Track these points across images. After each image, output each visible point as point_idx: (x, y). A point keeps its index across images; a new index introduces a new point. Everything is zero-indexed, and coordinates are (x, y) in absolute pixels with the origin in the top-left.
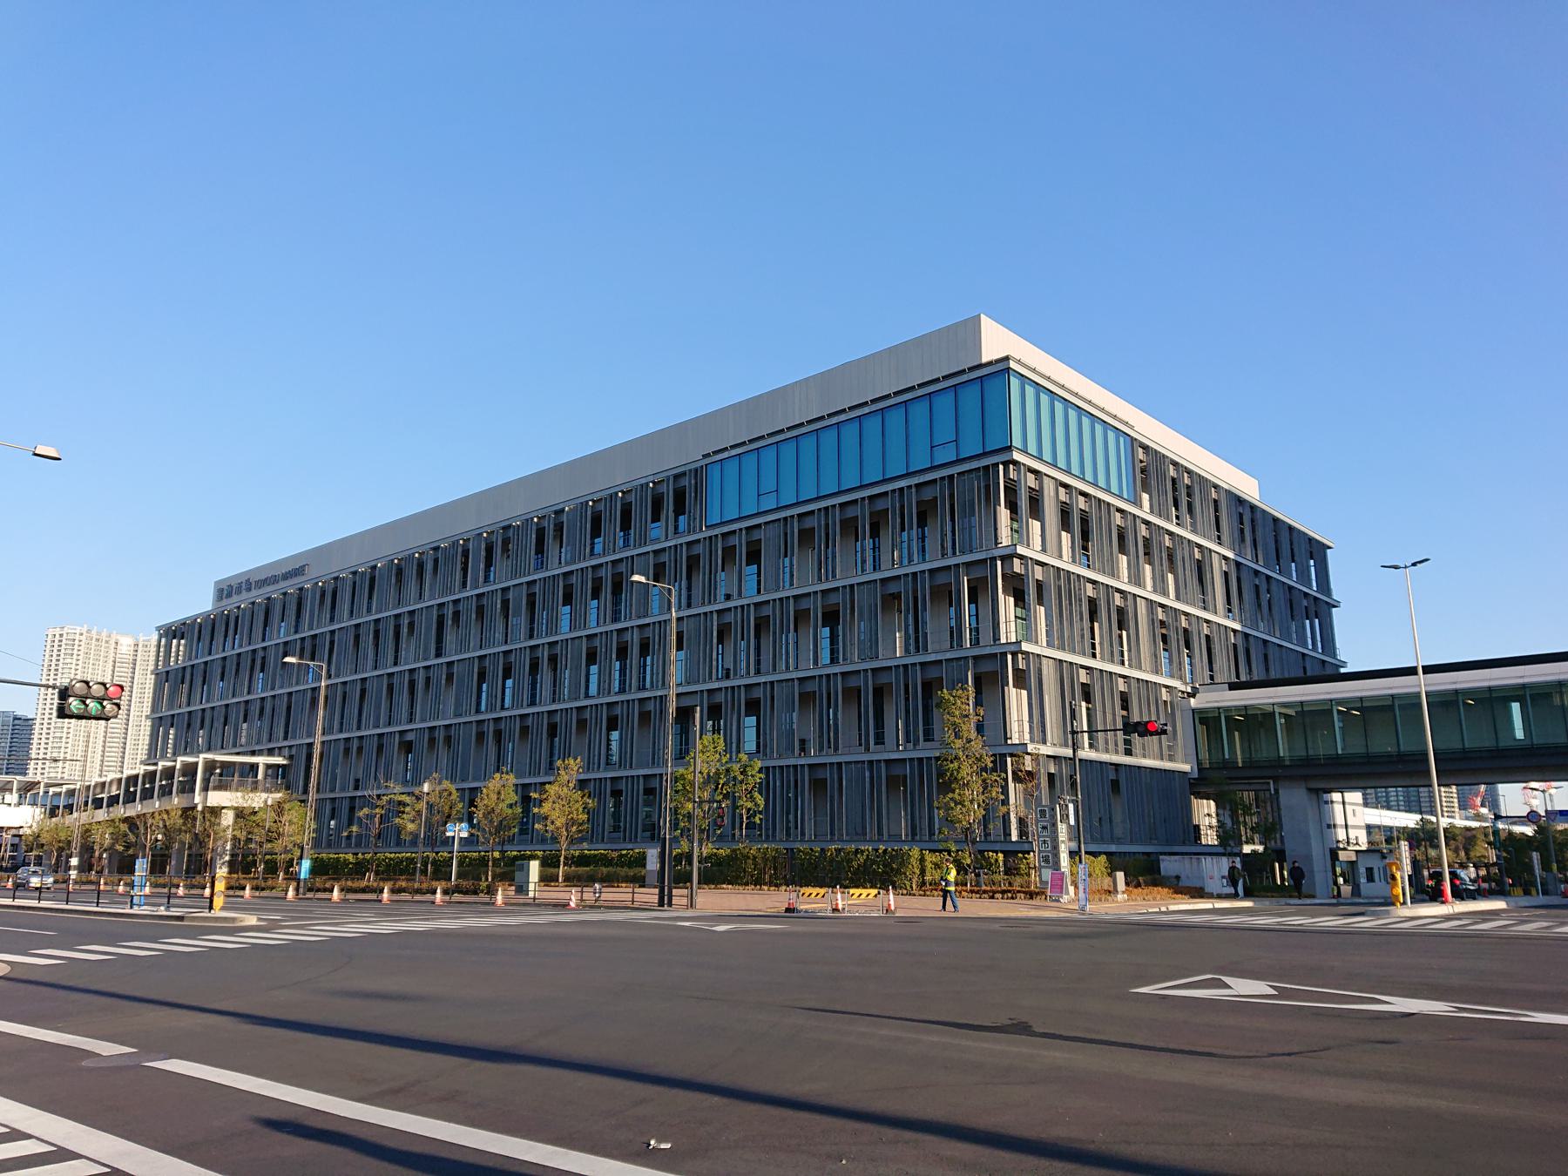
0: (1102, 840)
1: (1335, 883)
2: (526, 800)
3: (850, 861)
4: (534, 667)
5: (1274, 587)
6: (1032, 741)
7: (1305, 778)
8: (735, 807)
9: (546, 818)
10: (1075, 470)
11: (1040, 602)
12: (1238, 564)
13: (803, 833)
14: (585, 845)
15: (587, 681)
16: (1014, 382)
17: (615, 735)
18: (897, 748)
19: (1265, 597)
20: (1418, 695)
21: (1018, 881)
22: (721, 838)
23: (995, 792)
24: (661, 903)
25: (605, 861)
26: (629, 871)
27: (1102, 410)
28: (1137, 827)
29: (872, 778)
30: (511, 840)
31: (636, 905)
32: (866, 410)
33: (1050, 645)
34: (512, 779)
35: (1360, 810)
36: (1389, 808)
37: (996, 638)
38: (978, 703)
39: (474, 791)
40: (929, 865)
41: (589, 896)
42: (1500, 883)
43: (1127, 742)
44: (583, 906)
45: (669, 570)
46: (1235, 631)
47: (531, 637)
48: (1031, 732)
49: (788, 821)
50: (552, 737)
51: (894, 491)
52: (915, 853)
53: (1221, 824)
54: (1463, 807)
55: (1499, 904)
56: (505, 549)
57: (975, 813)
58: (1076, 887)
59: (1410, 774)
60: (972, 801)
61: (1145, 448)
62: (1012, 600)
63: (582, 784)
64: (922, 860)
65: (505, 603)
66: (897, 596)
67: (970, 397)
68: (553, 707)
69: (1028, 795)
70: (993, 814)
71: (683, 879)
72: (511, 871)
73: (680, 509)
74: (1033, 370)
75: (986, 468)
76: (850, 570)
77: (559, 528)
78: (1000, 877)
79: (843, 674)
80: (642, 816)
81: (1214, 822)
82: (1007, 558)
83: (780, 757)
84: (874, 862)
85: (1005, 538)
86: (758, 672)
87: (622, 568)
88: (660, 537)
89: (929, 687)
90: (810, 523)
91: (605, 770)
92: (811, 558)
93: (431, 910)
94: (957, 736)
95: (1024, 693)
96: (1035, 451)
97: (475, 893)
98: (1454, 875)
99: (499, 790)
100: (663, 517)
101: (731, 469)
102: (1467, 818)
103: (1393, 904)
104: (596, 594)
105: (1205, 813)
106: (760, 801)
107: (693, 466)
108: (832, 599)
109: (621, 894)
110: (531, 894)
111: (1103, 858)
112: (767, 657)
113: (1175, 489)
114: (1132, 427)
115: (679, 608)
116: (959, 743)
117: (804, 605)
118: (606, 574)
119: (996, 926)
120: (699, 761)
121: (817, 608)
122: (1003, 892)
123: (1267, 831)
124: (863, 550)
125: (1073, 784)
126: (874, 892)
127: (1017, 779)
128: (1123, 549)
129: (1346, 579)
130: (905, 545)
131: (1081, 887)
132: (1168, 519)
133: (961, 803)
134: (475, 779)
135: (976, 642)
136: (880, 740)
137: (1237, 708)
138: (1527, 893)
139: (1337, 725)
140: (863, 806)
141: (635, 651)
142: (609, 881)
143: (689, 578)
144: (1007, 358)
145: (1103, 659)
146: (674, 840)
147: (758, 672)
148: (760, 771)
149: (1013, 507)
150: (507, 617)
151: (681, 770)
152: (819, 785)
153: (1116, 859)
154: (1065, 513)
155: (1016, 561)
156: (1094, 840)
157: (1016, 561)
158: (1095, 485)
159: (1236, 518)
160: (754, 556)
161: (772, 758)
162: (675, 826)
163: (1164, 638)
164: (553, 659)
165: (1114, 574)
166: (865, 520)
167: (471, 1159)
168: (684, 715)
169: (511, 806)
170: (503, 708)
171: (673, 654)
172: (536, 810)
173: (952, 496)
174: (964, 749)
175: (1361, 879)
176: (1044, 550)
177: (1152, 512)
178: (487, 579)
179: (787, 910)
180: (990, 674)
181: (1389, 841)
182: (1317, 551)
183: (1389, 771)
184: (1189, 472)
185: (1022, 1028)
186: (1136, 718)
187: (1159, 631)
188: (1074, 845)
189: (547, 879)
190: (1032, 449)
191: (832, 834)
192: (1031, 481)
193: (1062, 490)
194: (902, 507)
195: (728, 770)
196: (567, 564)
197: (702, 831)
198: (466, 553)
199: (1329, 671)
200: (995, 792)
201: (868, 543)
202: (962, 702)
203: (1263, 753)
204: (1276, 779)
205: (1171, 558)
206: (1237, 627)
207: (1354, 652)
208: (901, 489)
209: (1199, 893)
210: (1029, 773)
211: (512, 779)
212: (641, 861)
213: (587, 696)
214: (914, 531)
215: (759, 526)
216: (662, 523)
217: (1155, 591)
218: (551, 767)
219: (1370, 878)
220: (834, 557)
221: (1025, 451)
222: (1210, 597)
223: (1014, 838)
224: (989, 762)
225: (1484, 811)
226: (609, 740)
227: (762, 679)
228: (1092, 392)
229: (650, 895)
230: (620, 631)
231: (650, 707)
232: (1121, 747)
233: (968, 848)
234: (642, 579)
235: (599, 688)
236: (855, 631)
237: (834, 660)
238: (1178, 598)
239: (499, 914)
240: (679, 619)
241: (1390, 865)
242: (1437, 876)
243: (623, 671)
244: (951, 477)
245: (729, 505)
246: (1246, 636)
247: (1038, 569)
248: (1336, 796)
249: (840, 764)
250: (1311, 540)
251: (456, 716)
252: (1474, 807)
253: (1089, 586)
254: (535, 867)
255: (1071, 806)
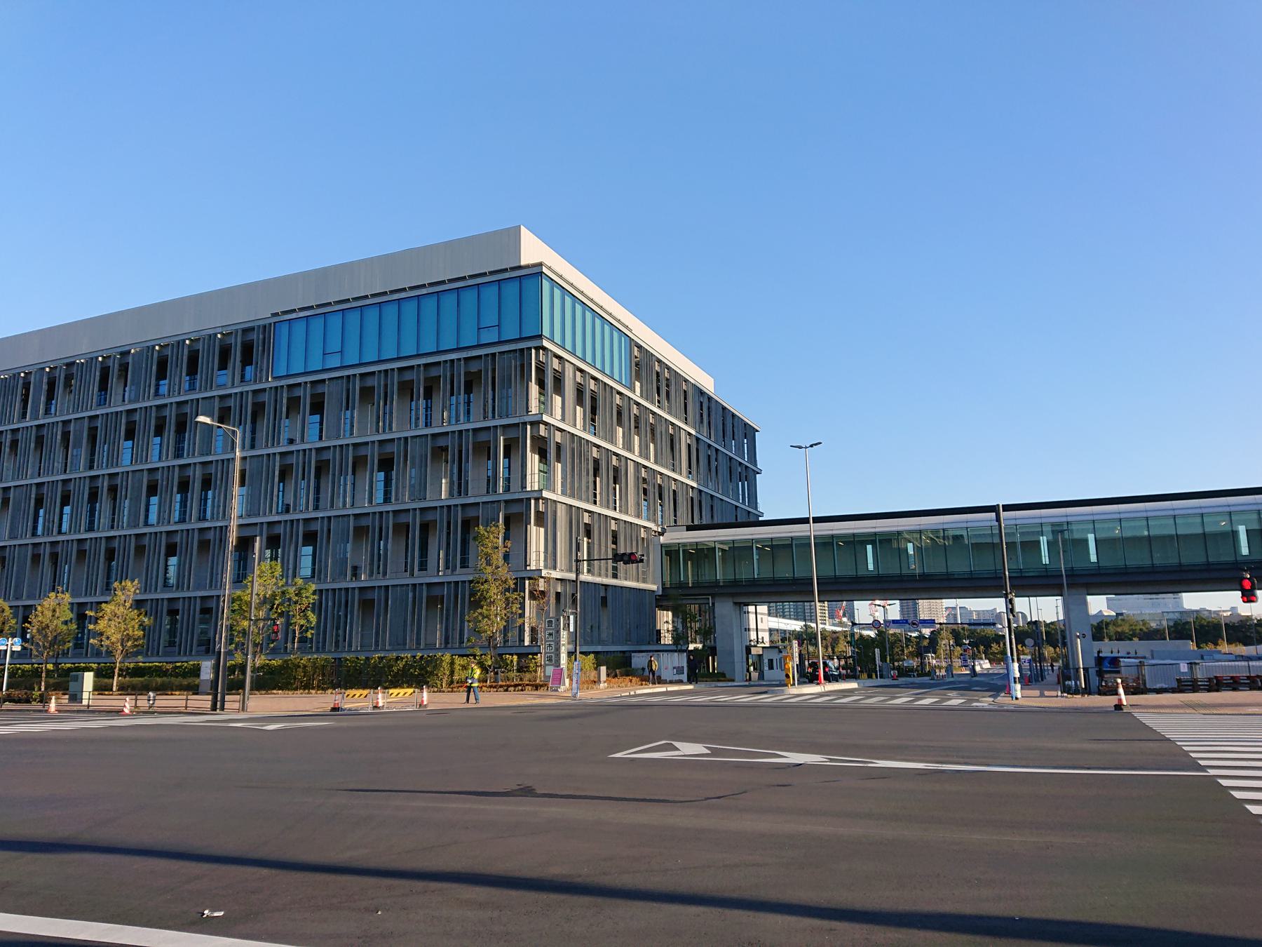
0: (592, 643)
1: (748, 670)
2: (81, 618)
3: (390, 667)
4: (94, 496)
5: (720, 458)
6: (546, 567)
7: (732, 595)
8: (288, 624)
9: (101, 634)
10: (589, 359)
11: (558, 459)
12: (698, 439)
13: (349, 644)
14: (140, 658)
15: (147, 510)
16: (546, 284)
17: (173, 561)
18: (438, 573)
19: (714, 463)
20: (809, 538)
21: (528, 676)
22: (274, 651)
23: (515, 607)
24: (214, 708)
25: (160, 672)
26: (187, 681)
27: (610, 314)
28: (617, 632)
29: (414, 598)
30: (65, 654)
31: (189, 710)
32: (424, 291)
33: (564, 493)
34: (67, 598)
35: (765, 618)
36: (784, 617)
37: (524, 486)
38: (506, 538)
39: (28, 608)
40: (457, 667)
41: (143, 703)
42: (854, 670)
43: (615, 569)
44: (137, 712)
45: (235, 414)
46: (693, 488)
47: (91, 468)
48: (546, 560)
49: (337, 635)
50: (111, 561)
51: (445, 362)
52: (447, 657)
53: (675, 629)
54: (831, 617)
55: (853, 685)
56: (68, 384)
57: (499, 623)
58: (571, 680)
59: (800, 593)
60: (496, 616)
61: (639, 347)
62: (537, 457)
63: (138, 604)
64: (452, 663)
65: (66, 436)
66: (445, 449)
67: (511, 290)
68: (112, 533)
69: (540, 610)
70: (512, 625)
71: (236, 687)
72: (65, 682)
73: (247, 359)
74: (561, 277)
75: (522, 350)
76: (404, 425)
77: (124, 368)
78: (513, 674)
79: (394, 512)
80: (197, 632)
81: (670, 627)
82: (536, 424)
83: (333, 581)
84: (412, 666)
85: (534, 407)
86: (316, 508)
87: (187, 409)
88: (227, 384)
89: (468, 525)
90: (370, 382)
91: (162, 592)
92: (370, 412)
93: (44, 715)
94: (489, 564)
95: (542, 530)
96: (559, 340)
97: (28, 701)
98: (825, 665)
99: (54, 609)
100: (230, 365)
101: (300, 328)
102: (834, 625)
103: (786, 685)
104: (159, 431)
105: (665, 620)
106: (313, 618)
107: (261, 323)
108: (389, 448)
109: (176, 700)
110: (85, 702)
111: (592, 656)
112: (326, 495)
113: (658, 380)
114: (630, 331)
115: (243, 448)
116: (489, 569)
117: (362, 451)
118: (171, 415)
119: (509, 713)
120: (256, 585)
121: (374, 455)
122: (516, 686)
123: (707, 633)
124: (417, 409)
125: (574, 601)
126: (410, 691)
127: (532, 597)
128: (620, 423)
129: (767, 453)
130: (454, 407)
131: (575, 679)
132: (652, 403)
133: (488, 617)
134: (29, 597)
135: (507, 489)
136: (423, 566)
137: (691, 544)
138: (870, 677)
139: (756, 557)
140: (405, 622)
141: (197, 486)
142: (163, 689)
143: (254, 422)
144: (541, 264)
145: (601, 506)
146: (229, 653)
147: (316, 508)
148: (314, 593)
149: (541, 384)
150: (67, 448)
151: (239, 593)
152: (367, 605)
153: (601, 656)
154: (580, 392)
155: (542, 427)
156: (586, 643)
157: (542, 427)
158: (603, 372)
159: (698, 405)
160: (317, 408)
161: (325, 582)
162: (230, 640)
163: (645, 494)
164: (113, 490)
165: (612, 441)
166: (422, 383)
167: (38, 940)
168: (245, 544)
169: (66, 623)
170: (60, 532)
171: (236, 489)
172: (91, 627)
173: (494, 370)
174: (493, 573)
175: (762, 668)
176: (563, 420)
177: (641, 396)
178: (47, 412)
179: (334, 709)
180: (517, 516)
181: (783, 640)
182: (749, 432)
183: (785, 590)
184: (669, 368)
185: (527, 792)
186: (622, 551)
187: (642, 486)
188: (571, 647)
189: (100, 689)
190: (557, 339)
191: (377, 645)
192: (556, 363)
193: (578, 374)
194: (452, 376)
195: (283, 593)
196: (130, 402)
197: (256, 645)
198: (27, 386)
199: (752, 519)
200: (515, 607)
201: (422, 402)
202: (494, 537)
203: (707, 577)
204: (713, 596)
205: (653, 431)
206: (695, 485)
207: (769, 507)
208: (452, 361)
209: (660, 681)
210: (543, 593)
211: (67, 598)
212: (196, 671)
213: (146, 524)
214: (462, 396)
215: (323, 381)
216: (229, 371)
217: (641, 456)
218: (108, 588)
219: (771, 667)
220: (391, 413)
221: (552, 340)
222: (677, 463)
223: (527, 643)
224: (511, 584)
225: (845, 619)
226: (166, 566)
227: (320, 515)
228: (607, 300)
229: (205, 701)
230: (182, 467)
231: (210, 535)
232: (610, 572)
233: (490, 652)
234: (207, 420)
235: (159, 517)
236: (407, 475)
237: (387, 499)
238: (656, 462)
239: (51, 720)
240: (244, 459)
241: (785, 658)
242: (815, 666)
243: (184, 503)
244: (494, 355)
245: (294, 360)
246: (700, 491)
247: (558, 434)
248: (752, 608)
249: (387, 587)
250: (746, 424)
251: (11, 538)
252: (839, 617)
253: (595, 449)
254: (89, 678)
255: (572, 617)
